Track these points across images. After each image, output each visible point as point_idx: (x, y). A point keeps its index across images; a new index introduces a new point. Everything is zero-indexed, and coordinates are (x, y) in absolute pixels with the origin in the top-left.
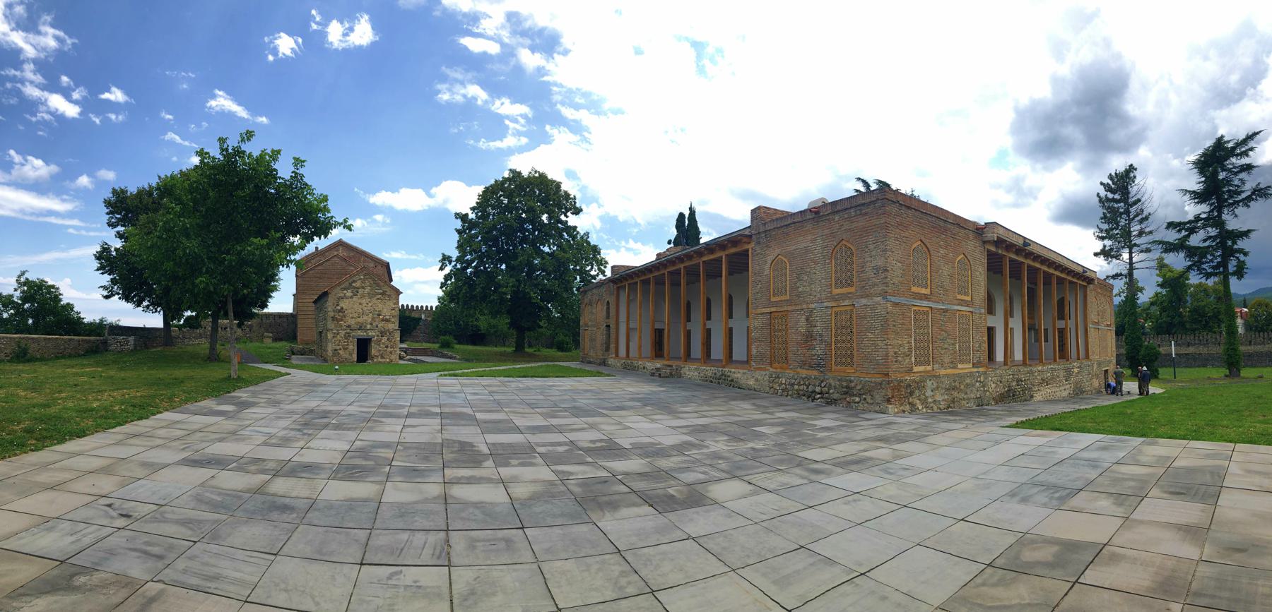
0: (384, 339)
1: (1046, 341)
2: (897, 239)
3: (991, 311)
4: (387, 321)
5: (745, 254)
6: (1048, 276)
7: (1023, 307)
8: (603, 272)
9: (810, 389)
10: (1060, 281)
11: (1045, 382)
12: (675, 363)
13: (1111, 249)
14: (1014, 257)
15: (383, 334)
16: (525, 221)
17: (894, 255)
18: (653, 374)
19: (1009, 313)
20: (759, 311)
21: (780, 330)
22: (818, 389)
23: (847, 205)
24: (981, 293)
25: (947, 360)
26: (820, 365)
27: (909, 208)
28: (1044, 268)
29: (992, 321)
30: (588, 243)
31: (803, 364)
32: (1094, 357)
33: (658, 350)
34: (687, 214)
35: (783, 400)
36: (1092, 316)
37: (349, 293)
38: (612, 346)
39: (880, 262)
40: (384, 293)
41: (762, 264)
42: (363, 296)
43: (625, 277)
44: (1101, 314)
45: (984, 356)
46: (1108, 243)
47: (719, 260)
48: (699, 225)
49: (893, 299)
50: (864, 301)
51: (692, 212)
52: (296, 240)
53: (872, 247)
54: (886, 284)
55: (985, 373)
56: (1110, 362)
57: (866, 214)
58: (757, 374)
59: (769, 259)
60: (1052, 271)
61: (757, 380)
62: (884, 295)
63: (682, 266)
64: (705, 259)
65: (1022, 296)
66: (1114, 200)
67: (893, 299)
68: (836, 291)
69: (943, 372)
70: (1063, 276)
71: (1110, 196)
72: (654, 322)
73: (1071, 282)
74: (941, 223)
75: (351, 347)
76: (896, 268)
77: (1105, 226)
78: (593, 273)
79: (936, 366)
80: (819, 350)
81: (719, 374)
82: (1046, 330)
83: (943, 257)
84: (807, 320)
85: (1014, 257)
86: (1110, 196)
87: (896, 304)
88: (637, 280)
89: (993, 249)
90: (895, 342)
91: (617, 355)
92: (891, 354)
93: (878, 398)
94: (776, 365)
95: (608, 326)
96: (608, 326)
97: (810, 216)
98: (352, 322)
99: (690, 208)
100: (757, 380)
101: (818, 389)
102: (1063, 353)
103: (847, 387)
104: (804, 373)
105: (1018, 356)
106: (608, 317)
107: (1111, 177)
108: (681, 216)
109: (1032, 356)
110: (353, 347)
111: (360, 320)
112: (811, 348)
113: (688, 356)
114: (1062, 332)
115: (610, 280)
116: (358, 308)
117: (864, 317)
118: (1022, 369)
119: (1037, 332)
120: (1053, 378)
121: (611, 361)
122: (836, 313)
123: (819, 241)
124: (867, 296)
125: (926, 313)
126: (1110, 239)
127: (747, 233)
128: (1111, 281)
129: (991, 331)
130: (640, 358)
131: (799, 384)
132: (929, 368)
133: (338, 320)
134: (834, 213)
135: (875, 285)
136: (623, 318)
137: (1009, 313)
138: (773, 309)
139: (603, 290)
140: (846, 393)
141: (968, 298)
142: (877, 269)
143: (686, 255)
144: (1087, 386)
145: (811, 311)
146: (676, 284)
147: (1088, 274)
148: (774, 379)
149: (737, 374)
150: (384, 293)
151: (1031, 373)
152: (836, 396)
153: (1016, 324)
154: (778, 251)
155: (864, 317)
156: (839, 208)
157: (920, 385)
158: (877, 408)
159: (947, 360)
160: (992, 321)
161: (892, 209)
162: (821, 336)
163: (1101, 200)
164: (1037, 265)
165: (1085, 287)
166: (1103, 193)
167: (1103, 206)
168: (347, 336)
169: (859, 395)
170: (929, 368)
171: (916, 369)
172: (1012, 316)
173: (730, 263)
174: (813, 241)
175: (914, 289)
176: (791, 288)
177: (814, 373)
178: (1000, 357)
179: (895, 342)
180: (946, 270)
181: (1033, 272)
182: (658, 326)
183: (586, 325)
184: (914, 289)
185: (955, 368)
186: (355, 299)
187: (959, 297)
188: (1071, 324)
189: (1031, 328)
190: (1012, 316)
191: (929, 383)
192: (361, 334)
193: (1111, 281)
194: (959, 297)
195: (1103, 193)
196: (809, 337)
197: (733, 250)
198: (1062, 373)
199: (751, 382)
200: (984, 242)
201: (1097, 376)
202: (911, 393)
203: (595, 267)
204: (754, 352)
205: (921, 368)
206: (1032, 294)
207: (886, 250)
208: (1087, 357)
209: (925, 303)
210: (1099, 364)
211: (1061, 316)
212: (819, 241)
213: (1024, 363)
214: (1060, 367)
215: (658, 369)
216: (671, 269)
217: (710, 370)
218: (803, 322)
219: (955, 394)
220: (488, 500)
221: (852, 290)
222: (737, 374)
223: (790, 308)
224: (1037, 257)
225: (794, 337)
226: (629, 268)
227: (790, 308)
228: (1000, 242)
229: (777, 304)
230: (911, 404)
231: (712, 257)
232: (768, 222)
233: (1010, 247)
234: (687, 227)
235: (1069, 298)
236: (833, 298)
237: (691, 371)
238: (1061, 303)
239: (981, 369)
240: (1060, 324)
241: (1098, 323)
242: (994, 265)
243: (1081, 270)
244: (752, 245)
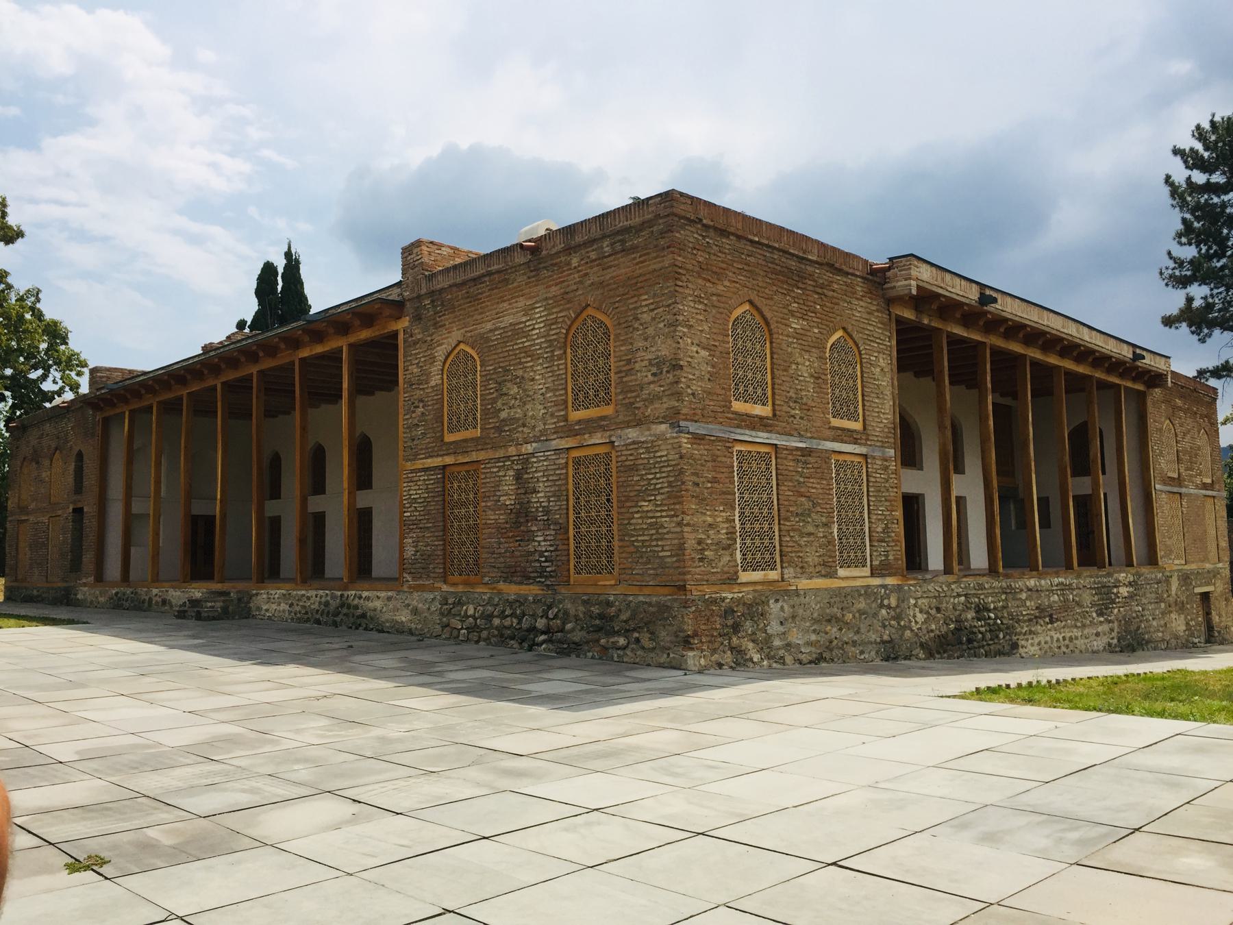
1: (1045, 523)
2: (698, 300)
3: (910, 457)
5: (389, 344)
6: (1043, 373)
7: (984, 442)
8: (75, 387)
9: (525, 624)
10: (1077, 384)
11: (1047, 615)
12: (233, 588)
13: (1209, 307)
14: (958, 331)
17: (695, 334)
18: (181, 615)
19: (953, 463)
20: (419, 464)
21: (464, 504)
22: (541, 623)
23: (595, 232)
24: (885, 412)
25: (812, 558)
26: (550, 574)
27: (723, 233)
28: (1035, 354)
29: (912, 482)
30: (38, 315)
31: (513, 573)
32: (1172, 563)
33: (200, 556)
34: (280, 264)
35: (469, 650)
36: (1164, 463)
38: (88, 558)
39: (664, 349)
41: (429, 362)
43: (122, 395)
44: (1185, 457)
45: (897, 552)
46: (1199, 292)
47: (335, 356)
48: (308, 290)
49: (693, 427)
50: (632, 434)
51: (293, 264)
53: (646, 317)
54: (678, 395)
55: (899, 588)
56: (1215, 573)
57: (634, 249)
58: (416, 599)
59: (440, 353)
60: (1053, 360)
61: (415, 611)
62: (673, 418)
63: (254, 370)
64: (305, 353)
65: (983, 419)
66: (1209, 188)
67: (693, 427)
68: (575, 415)
69: (804, 584)
70: (1081, 369)
71: (1199, 178)
72: (189, 497)
73: (1103, 385)
74: (793, 264)
76: (697, 357)
77: (1189, 252)
78: (47, 386)
79: (789, 572)
80: (542, 541)
81: (334, 604)
82: (1044, 502)
83: (798, 335)
84: (518, 477)
85: (958, 331)
86: (1199, 178)
87: (697, 438)
88: (153, 401)
89: (909, 314)
90: (698, 519)
91: (99, 578)
92: (691, 543)
93: (664, 636)
94: (456, 578)
95: (78, 511)
96: (78, 511)
97: (520, 259)
99: (288, 255)
100: (415, 611)
101: (541, 623)
102: (1090, 554)
103: (601, 616)
104: (512, 590)
105: (978, 557)
106: (78, 488)
107: (1200, 133)
108: (269, 269)
109: (1012, 553)
112: (528, 537)
113: (271, 571)
114: (1086, 506)
115: (81, 401)
117: (633, 468)
118: (987, 582)
119: (1023, 506)
120: (1066, 607)
121: (83, 593)
122: (578, 462)
123: (539, 312)
124: (639, 423)
125: (765, 458)
126: (1203, 282)
127: (394, 295)
128: (1213, 382)
129: (912, 505)
130: (156, 579)
131: (502, 616)
132: (773, 575)
134: (569, 250)
135: (651, 400)
136: (116, 489)
137: (953, 463)
138: (449, 460)
139: (68, 425)
140: (599, 629)
141: (857, 426)
142: (658, 363)
143: (263, 346)
144: (1153, 627)
145: (526, 460)
146: (239, 412)
147: (1148, 361)
148: (451, 607)
149: (375, 600)
151: (1010, 592)
152: (578, 636)
153: (970, 486)
154: (457, 335)
155: (633, 468)
156: (579, 239)
157: (755, 609)
158: (663, 659)
159: (812, 558)
160: (912, 482)
161: (689, 235)
162: (547, 511)
163: (1174, 190)
164: (1016, 347)
165: (1141, 398)
166: (1180, 173)
167: (1183, 205)
169: (627, 633)
170: (773, 575)
171: (745, 577)
172: (959, 470)
173: (356, 364)
174: (528, 310)
175: (738, 406)
176: (485, 412)
177: (532, 591)
178: (935, 557)
179: (698, 519)
180: (805, 366)
181: (1006, 364)
182: (199, 509)
183: (23, 510)
184: (738, 406)
185: (832, 575)
187: (836, 422)
188: (1106, 484)
189: (1008, 498)
190: (959, 470)
191: (774, 607)
193: (1213, 382)
194: (836, 422)
195: (1180, 173)
196: (522, 515)
197: (364, 334)
198: (1087, 598)
199: (404, 617)
200: (890, 302)
201: (1181, 607)
202: (736, 628)
203: (55, 373)
204: (409, 551)
205: (757, 576)
206: (1006, 420)
207: (673, 325)
208: (1152, 560)
209: (762, 437)
210: (1185, 578)
211: (1082, 465)
212: (539, 312)
213: (992, 571)
214: (1083, 582)
215: (194, 603)
216: (231, 375)
217: (314, 596)
218: (508, 484)
219: (833, 631)
221: (608, 410)
222: (375, 600)
223: (481, 456)
224: (1015, 329)
225: (492, 516)
226: (132, 374)
227: (481, 456)
228: (925, 299)
229: (458, 448)
230: (738, 651)
231: (319, 349)
232: (440, 285)
233: (948, 308)
234: (280, 290)
235: (1101, 421)
236: (570, 430)
237: (271, 600)
238: (1081, 437)
239: (890, 581)
240: (1079, 486)
241: (1179, 481)
242: (913, 353)
243: (1127, 353)
244: (404, 323)
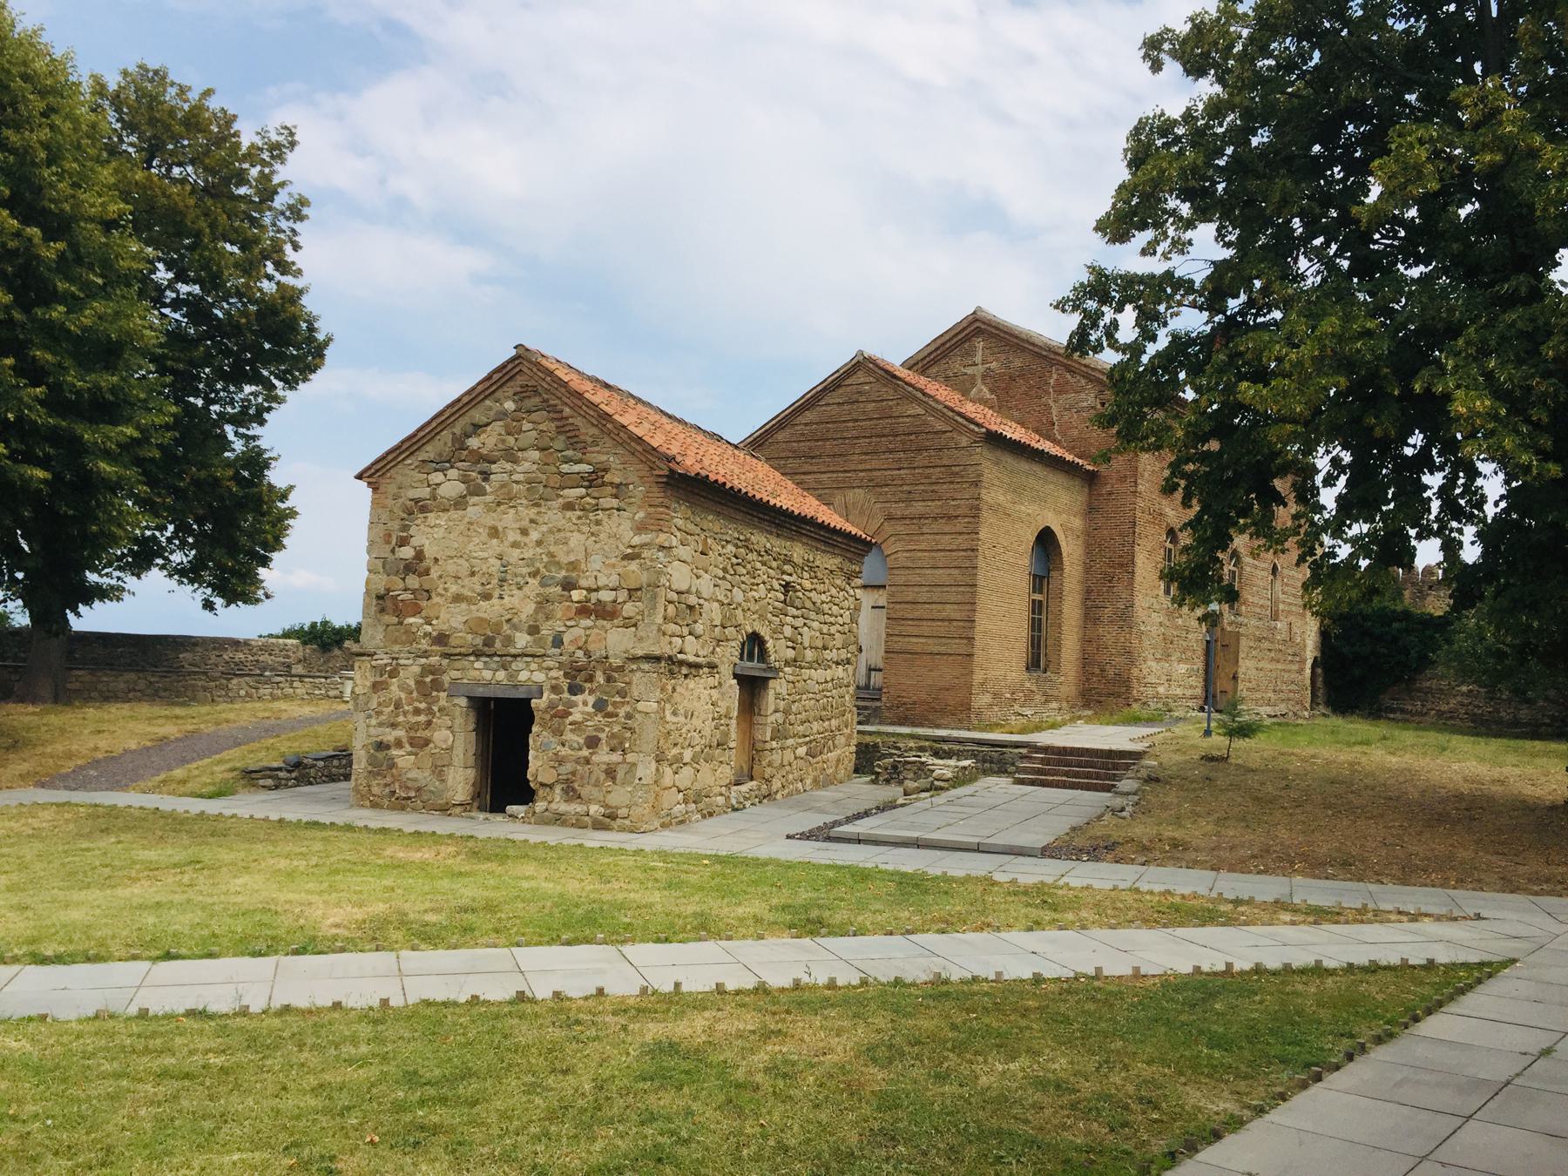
0: (583, 705)
4: (605, 612)
15: (577, 677)
16: (1559, 125)
27: (175, 866)
37: (450, 485)
40: (593, 480)
42: (506, 499)
52: (1520, 324)
75: (441, 736)
98: (451, 618)
110: (456, 739)
111: (490, 610)
116: (487, 554)
133: (400, 610)
150: (593, 480)
168: (429, 685)
186: (475, 508)
192: (487, 676)
220: (1300, 1100)
